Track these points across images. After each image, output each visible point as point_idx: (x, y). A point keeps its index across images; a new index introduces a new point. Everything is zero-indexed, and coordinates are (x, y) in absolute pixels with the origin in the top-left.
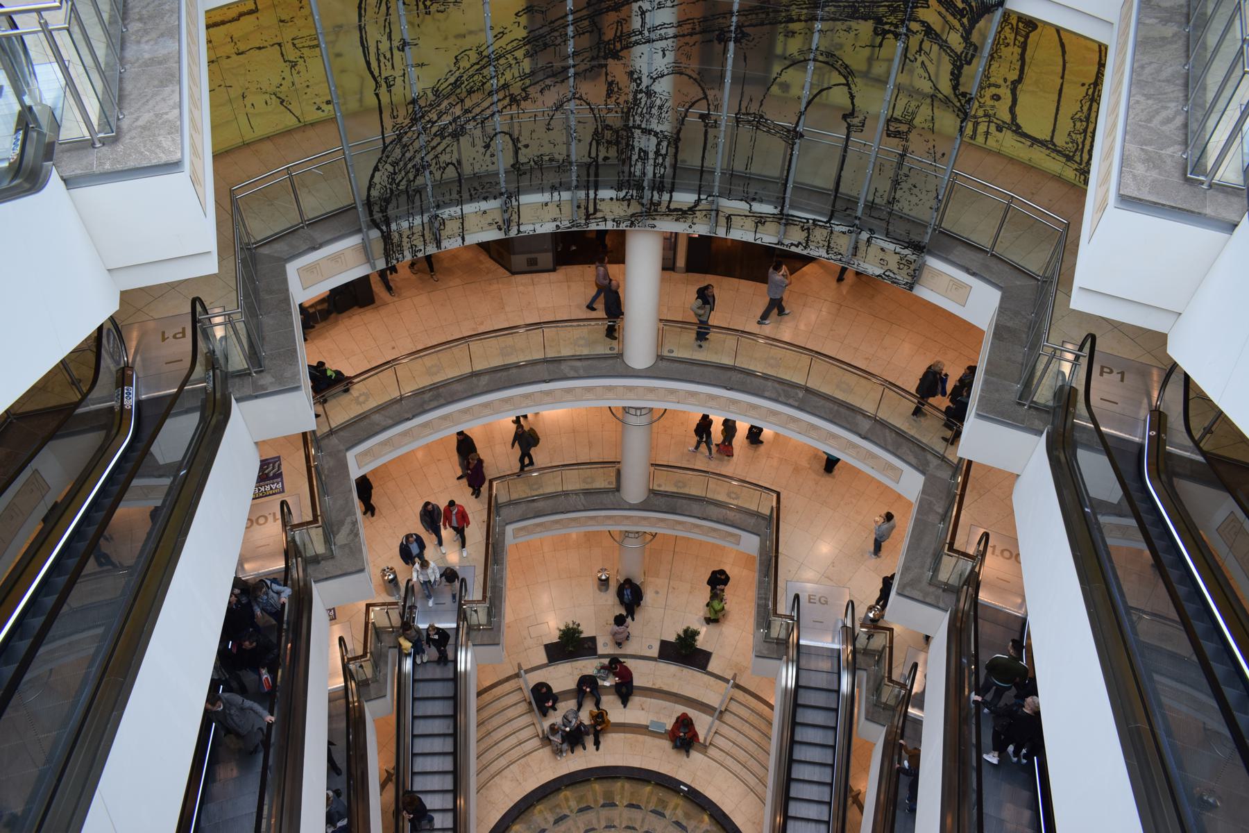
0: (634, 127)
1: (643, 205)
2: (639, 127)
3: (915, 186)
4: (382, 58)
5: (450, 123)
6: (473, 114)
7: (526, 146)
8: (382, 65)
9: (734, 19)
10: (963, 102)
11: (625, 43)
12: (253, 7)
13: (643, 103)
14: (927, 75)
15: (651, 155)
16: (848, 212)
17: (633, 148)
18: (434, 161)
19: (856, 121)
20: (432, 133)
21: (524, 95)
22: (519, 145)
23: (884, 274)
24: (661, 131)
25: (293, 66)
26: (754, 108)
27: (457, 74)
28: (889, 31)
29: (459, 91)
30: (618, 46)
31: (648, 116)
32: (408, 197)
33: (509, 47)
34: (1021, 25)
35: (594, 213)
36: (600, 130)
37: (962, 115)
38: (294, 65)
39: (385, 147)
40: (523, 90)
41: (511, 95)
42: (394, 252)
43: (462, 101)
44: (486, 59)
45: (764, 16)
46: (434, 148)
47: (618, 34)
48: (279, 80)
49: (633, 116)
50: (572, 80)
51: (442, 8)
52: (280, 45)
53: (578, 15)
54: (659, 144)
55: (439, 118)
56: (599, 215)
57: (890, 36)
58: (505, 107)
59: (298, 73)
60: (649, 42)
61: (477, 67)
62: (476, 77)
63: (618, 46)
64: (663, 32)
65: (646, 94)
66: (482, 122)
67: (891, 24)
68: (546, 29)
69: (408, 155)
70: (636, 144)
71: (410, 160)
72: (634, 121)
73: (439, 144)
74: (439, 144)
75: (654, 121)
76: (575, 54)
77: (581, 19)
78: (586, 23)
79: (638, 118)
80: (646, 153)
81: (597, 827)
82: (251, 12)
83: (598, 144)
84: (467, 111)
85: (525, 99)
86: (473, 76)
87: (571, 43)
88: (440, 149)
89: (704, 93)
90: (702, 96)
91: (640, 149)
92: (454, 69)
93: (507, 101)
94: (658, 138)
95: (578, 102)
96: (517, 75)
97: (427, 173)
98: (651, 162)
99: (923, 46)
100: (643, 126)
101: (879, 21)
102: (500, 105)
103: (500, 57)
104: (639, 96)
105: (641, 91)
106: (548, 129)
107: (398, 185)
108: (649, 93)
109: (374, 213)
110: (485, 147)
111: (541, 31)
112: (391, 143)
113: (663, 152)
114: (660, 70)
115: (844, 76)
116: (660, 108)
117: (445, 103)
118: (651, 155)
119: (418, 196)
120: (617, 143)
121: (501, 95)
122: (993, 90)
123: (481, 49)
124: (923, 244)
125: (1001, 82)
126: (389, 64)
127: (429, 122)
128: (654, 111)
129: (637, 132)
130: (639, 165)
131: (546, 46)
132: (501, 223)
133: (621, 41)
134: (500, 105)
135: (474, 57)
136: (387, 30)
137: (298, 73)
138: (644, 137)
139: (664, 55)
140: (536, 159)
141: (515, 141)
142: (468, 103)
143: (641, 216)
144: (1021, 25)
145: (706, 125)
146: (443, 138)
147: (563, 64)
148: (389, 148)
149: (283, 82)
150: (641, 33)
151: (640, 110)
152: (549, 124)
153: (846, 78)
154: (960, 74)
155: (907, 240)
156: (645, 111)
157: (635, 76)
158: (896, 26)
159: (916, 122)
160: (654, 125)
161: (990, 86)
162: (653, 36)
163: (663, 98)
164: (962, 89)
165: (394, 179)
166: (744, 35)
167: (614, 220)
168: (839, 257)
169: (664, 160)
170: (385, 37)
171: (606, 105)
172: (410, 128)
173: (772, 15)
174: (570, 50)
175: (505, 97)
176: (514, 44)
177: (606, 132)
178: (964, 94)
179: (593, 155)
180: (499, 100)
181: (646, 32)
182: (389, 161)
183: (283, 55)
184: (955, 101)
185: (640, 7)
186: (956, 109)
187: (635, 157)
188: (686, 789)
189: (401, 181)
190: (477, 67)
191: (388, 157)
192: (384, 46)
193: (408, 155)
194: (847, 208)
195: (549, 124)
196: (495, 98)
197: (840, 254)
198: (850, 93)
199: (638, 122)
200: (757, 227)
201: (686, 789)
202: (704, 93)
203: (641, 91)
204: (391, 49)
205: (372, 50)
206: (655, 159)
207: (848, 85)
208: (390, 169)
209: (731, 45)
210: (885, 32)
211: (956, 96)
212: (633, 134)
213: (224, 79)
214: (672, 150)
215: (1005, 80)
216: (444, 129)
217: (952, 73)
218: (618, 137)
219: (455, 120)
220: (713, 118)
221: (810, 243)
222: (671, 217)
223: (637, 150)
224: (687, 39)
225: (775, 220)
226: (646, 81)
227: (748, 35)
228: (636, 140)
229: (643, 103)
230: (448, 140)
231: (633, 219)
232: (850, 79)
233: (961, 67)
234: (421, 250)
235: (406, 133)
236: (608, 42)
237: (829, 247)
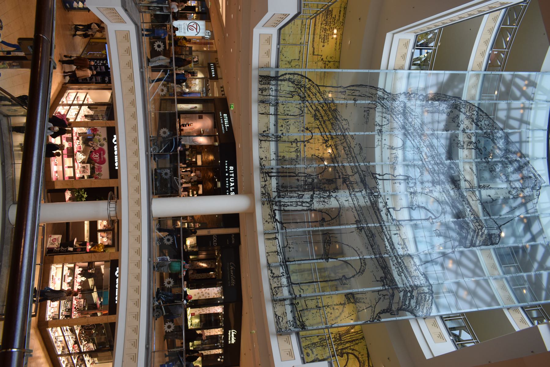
1: (275, 198)
2: (314, 193)
3: (331, 314)
4: (353, 91)
5: (321, 114)
6: (322, 124)
8: (351, 91)
9: (365, 225)
10: (377, 318)
11: (349, 185)
12: (315, 54)
13: (325, 194)
14: (377, 301)
15: (301, 200)
16: (302, 291)
17: (304, 192)
19: (344, 281)
20: (318, 107)
21: (328, 145)
22: (306, 143)
23: (279, 317)
25: (289, 62)
27: (340, 119)
28: (384, 282)
29: (334, 119)
30: (348, 183)
31: (319, 197)
32: (291, 92)
33: (348, 141)
34: (340, 351)
35: (269, 176)
36: (311, 177)
37: (371, 320)
38: (290, 63)
39: (318, 86)
40: (330, 145)
42: (266, 80)
44: (344, 131)
45: (370, 236)
46: (311, 106)
47: (352, 183)
48: (285, 56)
50: (333, 165)
51: (365, 117)
52: (299, 60)
53: (358, 167)
54: (307, 202)
55: (324, 110)
56: (268, 178)
57: (383, 283)
58: (323, 138)
59: (286, 64)
60: (350, 194)
61: (342, 127)
62: (338, 127)
63: (348, 183)
64: (355, 199)
65: (329, 195)
67: (387, 282)
68: (353, 155)
69: (311, 95)
70: (306, 193)
71: (309, 95)
72: (316, 191)
73: (313, 109)
74: (313, 109)
75: (318, 200)
76: (344, 166)
77: (357, 168)
78: (356, 170)
79: (318, 192)
80: (302, 197)
82: (313, 52)
83: (305, 176)
84: (324, 122)
85: (326, 146)
86: (339, 126)
87: (348, 165)
88: (310, 109)
89: (334, 218)
90: (333, 217)
91: (304, 195)
92: (342, 119)
93: (326, 139)
94: (310, 202)
96: (337, 143)
97: (300, 102)
98: (298, 200)
99: (386, 296)
100: (314, 195)
101: (386, 278)
102: (325, 136)
103: (344, 137)
104: (328, 192)
105: (330, 193)
107: (299, 88)
108: (329, 197)
109: (289, 75)
110: (307, 128)
111: (353, 153)
112: (319, 89)
113: (304, 205)
114: (340, 200)
115: (360, 271)
116: (324, 201)
117: (330, 113)
118: (301, 200)
119: (291, 96)
120: (305, 185)
121: (329, 136)
122: (310, 352)
123: (348, 130)
124: (306, 328)
125: (315, 353)
126: (350, 94)
127: (323, 106)
128: (322, 199)
129: (312, 193)
130: (296, 195)
131: (347, 155)
132: (267, 132)
133: (350, 183)
134: (325, 136)
135: (345, 127)
136: (362, 95)
137: (286, 64)
138: (309, 196)
139: (346, 201)
140: (299, 149)
141: (308, 141)
142: (327, 123)
143: (268, 198)
144: (340, 351)
146: (315, 111)
147: (340, 162)
148: (317, 87)
149: (284, 57)
150: (353, 191)
151: (322, 193)
153: (359, 272)
154: (386, 312)
155: (304, 320)
156: (321, 195)
158: (387, 284)
159: (357, 304)
160: (315, 200)
161: (311, 350)
162: (352, 196)
163: (329, 202)
164: (381, 315)
166: (361, 230)
167: (265, 185)
168: (275, 294)
169: (300, 205)
170: (360, 94)
172: (323, 98)
173: (371, 239)
174: (345, 164)
176: (349, 143)
178: (380, 317)
179: (300, 175)
180: (327, 135)
181: (353, 193)
182: (312, 86)
183: (294, 60)
184: (375, 315)
185: (363, 190)
186: (372, 317)
187: (300, 193)
189: (301, 90)
190: (342, 127)
191: (313, 86)
192: (357, 93)
193: (311, 95)
194: (303, 290)
196: (327, 134)
197: (277, 294)
198: (354, 275)
199: (316, 193)
200: (275, 252)
202: (334, 218)
203: (330, 193)
204: (355, 95)
205: (357, 88)
206: (299, 202)
207: (357, 273)
208: (307, 86)
209: (355, 226)
210: (383, 281)
211: (377, 314)
212: (311, 191)
213: (293, 34)
214: (305, 208)
215: (317, 355)
216: (319, 111)
217: (384, 310)
218: (309, 185)
219: (322, 116)
221: (276, 278)
222: (270, 212)
223: (303, 193)
224: (354, 209)
225: (282, 260)
226: (334, 195)
227: (361, 232)
229: (325, 194)
230: (313, 112)
231: (266, 194)
232: (360, 274)
233: (388, 312)
234: (262, 93)
235: (321, 96)
236: (349, 179)
237: (278, 287)
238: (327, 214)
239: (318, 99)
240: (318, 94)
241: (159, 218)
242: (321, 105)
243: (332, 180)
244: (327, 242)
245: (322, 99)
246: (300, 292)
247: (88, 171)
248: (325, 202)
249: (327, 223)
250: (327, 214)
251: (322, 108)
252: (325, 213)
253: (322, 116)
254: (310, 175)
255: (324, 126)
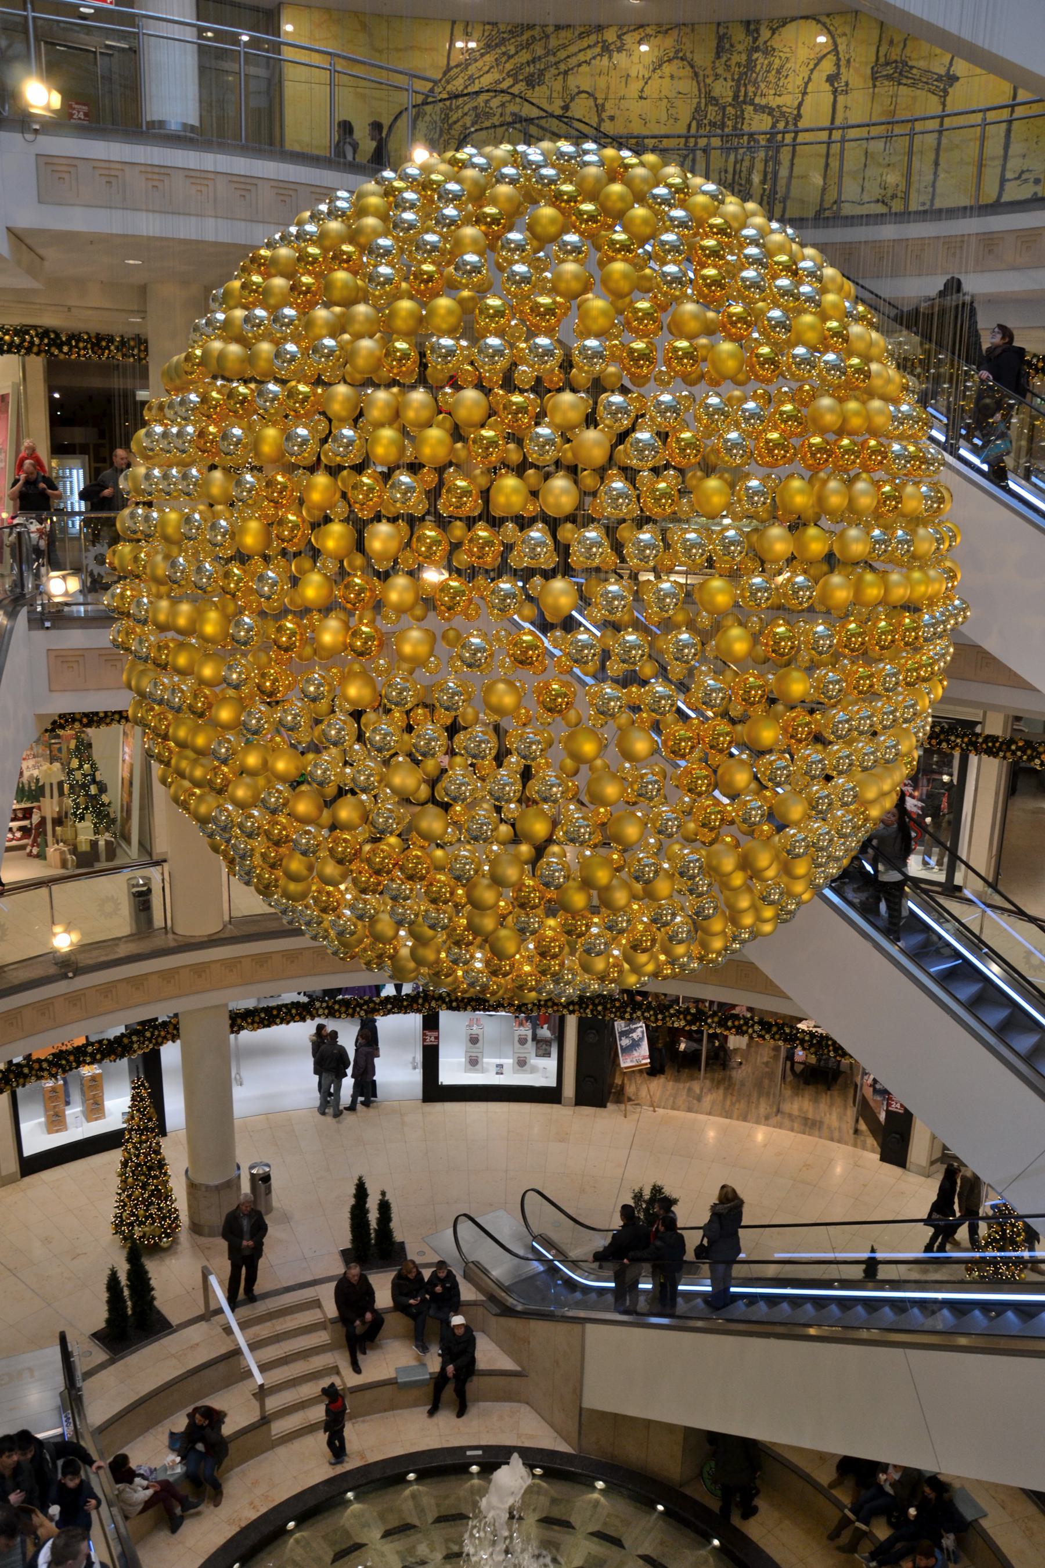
0: (744, 102)
5: (528, 63)
7: (612, 118)
16: (1024, 177)
18: (500, 110)
21: (619, 44)
24: (778, 107)
26: (895, 54)
41: (604, 41)
43: (547, 37)
49: (745, 85)
55: (517, 53)
66: (566, 73)
81: (416, 1521)
85: (620, 50)
93: (597, 50)
94: (773, 117)
95: (681, 64)
102: (589, 54)
106: (641, 98)
107: (450, 127)
112: (457, 66)
116: (778, 72)
127: (504, 54)
128: (772, 76)
145: (835, 92)
148: (452, 73)
152: (642, 91)
157: (752, 27)
165: (447, 117)
171: (714, 68)
172: (482, 55)
175: (595, 45)
177: (710, 108)
188: (480, 1452)
189: (455, 122)
191: (448, 82)
194: (1023, 172)
195: (642, 91)
201: (480, 1452)
212: (743, 111)
218: (724, 115)
219: (533, 61)
220: (844, 79)
228: (746, 121)
235: (476, 60)
238: (816, 65)
239: (486, 68)
240: (472, 69)
241: (1018, 719)
242: (504, 59)
243: (721, 39)
244: (900, 74)
245: (487, 58)
246: (1026, 181)
247: (329, 1029)
248: (782, 67)
249: (843, 70)
250: (816, 65)
251: (510, 57)
252: (812, 71)
253: (533, 61)
254: (697, 109)
255: (562, 54)
